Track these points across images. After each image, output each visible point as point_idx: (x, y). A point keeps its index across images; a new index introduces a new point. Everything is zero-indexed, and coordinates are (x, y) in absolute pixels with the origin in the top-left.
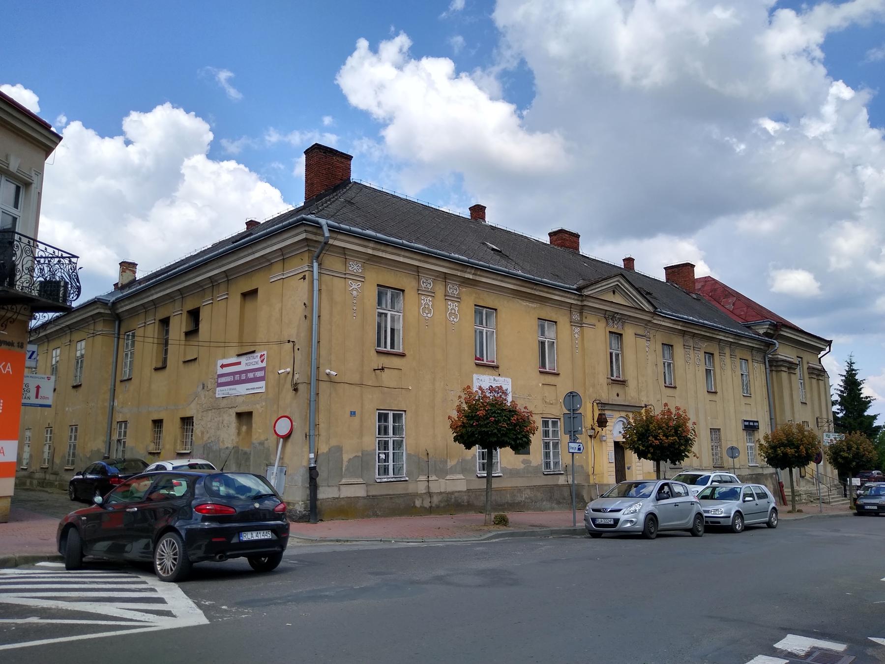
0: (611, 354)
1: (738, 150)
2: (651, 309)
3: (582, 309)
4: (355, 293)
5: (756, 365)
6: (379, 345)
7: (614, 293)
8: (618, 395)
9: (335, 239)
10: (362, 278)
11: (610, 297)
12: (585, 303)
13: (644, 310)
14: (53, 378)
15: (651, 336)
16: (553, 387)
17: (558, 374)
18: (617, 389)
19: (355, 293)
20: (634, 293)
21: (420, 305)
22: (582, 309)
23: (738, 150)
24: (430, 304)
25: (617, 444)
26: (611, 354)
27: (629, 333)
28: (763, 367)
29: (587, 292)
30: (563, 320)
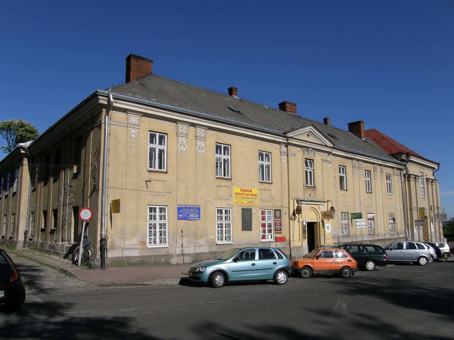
0: (306, 172)
1: (218, 276)
2: (331, 145)
3: (287, 145)
4: (133, 136)
5: (395, 177)
6: (151, 166)
7: (308, 135)
8: (310, 195)
9: (116, 102)
10: (137, 126)
11: (305, 138)
12: (289, 141)
13: (327, 146)
14: (413, 169)
15: (332, 161)
16: (269, 191)
17: (272, 183)
18: (309, 191)
19: (133, 136)
20: (321, 136)
21: (178, 142)
22: (287, 145)
23: (218, 276)
24: (185, 142)
25: (317, 259)
26: (306, 172)
27: (318, 157)
28: (399, 178)
29: (290, 135)
30: (274, 149)
